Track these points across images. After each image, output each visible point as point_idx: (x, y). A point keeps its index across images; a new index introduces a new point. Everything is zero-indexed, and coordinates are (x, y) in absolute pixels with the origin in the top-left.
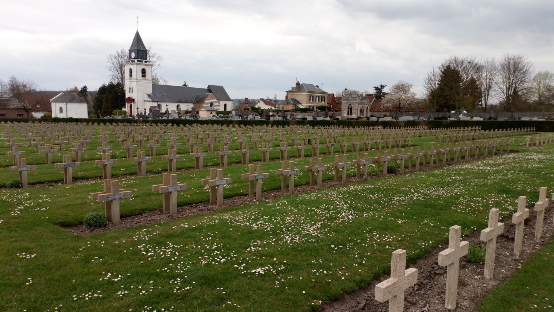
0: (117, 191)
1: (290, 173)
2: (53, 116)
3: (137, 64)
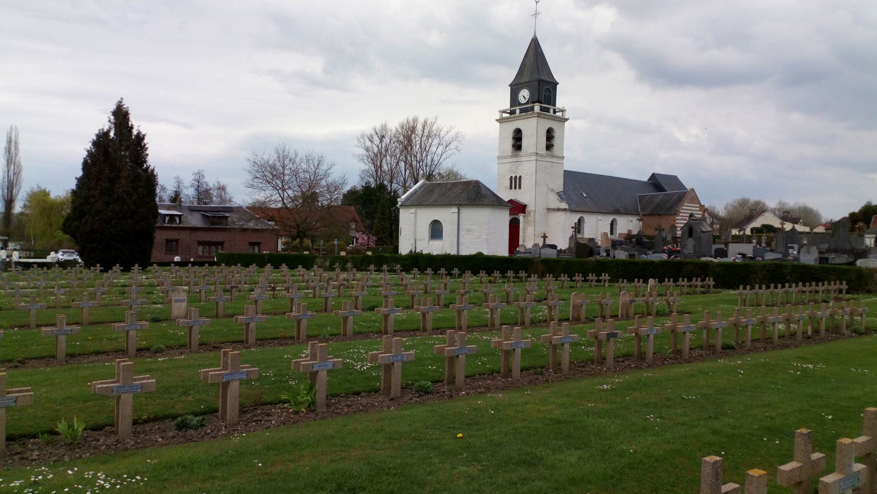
0: (324, 359)
1: (563, 341)
2: (404, 249)
3: (539, 116)
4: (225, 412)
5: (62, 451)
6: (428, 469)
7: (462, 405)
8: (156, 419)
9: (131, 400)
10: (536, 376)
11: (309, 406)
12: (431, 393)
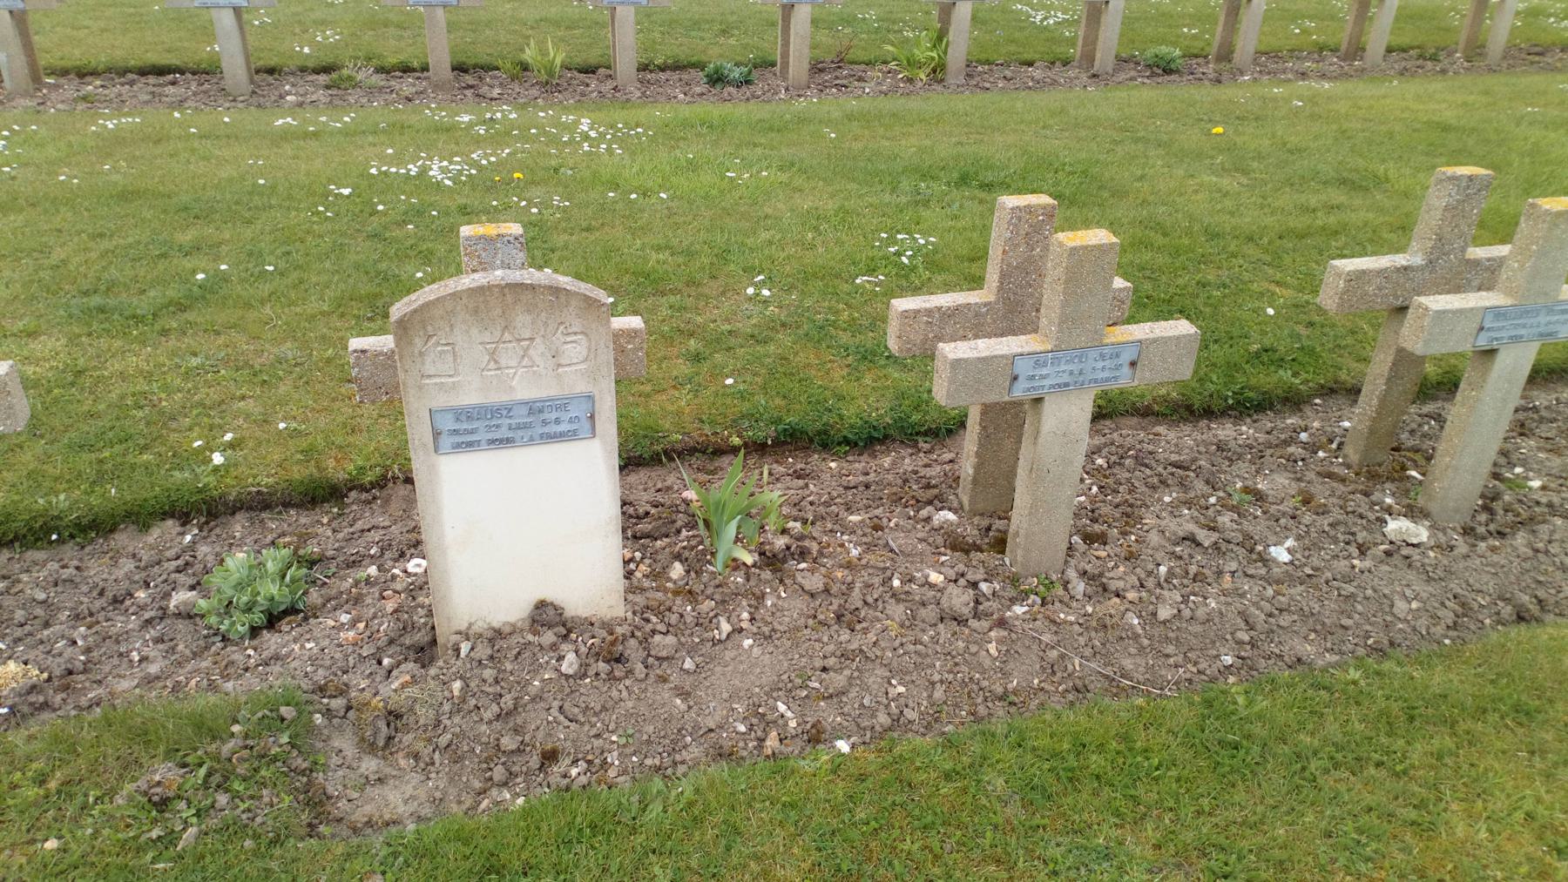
4: (785, 65)
5: (535, 92)
6: (1139, 173)
7: (1240, 93)
8: (678, 67)
9: (632, 18)
10: (1420, 62)
11: (934, 71)
12: (1177, 71)
